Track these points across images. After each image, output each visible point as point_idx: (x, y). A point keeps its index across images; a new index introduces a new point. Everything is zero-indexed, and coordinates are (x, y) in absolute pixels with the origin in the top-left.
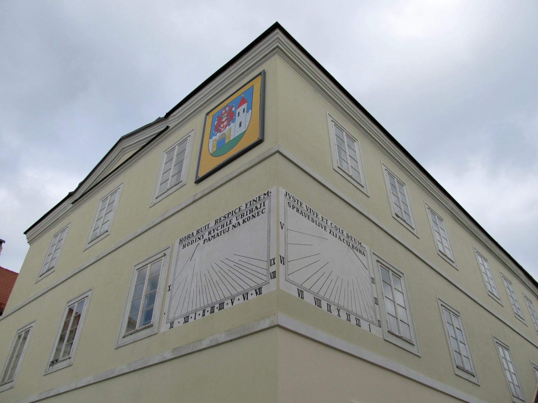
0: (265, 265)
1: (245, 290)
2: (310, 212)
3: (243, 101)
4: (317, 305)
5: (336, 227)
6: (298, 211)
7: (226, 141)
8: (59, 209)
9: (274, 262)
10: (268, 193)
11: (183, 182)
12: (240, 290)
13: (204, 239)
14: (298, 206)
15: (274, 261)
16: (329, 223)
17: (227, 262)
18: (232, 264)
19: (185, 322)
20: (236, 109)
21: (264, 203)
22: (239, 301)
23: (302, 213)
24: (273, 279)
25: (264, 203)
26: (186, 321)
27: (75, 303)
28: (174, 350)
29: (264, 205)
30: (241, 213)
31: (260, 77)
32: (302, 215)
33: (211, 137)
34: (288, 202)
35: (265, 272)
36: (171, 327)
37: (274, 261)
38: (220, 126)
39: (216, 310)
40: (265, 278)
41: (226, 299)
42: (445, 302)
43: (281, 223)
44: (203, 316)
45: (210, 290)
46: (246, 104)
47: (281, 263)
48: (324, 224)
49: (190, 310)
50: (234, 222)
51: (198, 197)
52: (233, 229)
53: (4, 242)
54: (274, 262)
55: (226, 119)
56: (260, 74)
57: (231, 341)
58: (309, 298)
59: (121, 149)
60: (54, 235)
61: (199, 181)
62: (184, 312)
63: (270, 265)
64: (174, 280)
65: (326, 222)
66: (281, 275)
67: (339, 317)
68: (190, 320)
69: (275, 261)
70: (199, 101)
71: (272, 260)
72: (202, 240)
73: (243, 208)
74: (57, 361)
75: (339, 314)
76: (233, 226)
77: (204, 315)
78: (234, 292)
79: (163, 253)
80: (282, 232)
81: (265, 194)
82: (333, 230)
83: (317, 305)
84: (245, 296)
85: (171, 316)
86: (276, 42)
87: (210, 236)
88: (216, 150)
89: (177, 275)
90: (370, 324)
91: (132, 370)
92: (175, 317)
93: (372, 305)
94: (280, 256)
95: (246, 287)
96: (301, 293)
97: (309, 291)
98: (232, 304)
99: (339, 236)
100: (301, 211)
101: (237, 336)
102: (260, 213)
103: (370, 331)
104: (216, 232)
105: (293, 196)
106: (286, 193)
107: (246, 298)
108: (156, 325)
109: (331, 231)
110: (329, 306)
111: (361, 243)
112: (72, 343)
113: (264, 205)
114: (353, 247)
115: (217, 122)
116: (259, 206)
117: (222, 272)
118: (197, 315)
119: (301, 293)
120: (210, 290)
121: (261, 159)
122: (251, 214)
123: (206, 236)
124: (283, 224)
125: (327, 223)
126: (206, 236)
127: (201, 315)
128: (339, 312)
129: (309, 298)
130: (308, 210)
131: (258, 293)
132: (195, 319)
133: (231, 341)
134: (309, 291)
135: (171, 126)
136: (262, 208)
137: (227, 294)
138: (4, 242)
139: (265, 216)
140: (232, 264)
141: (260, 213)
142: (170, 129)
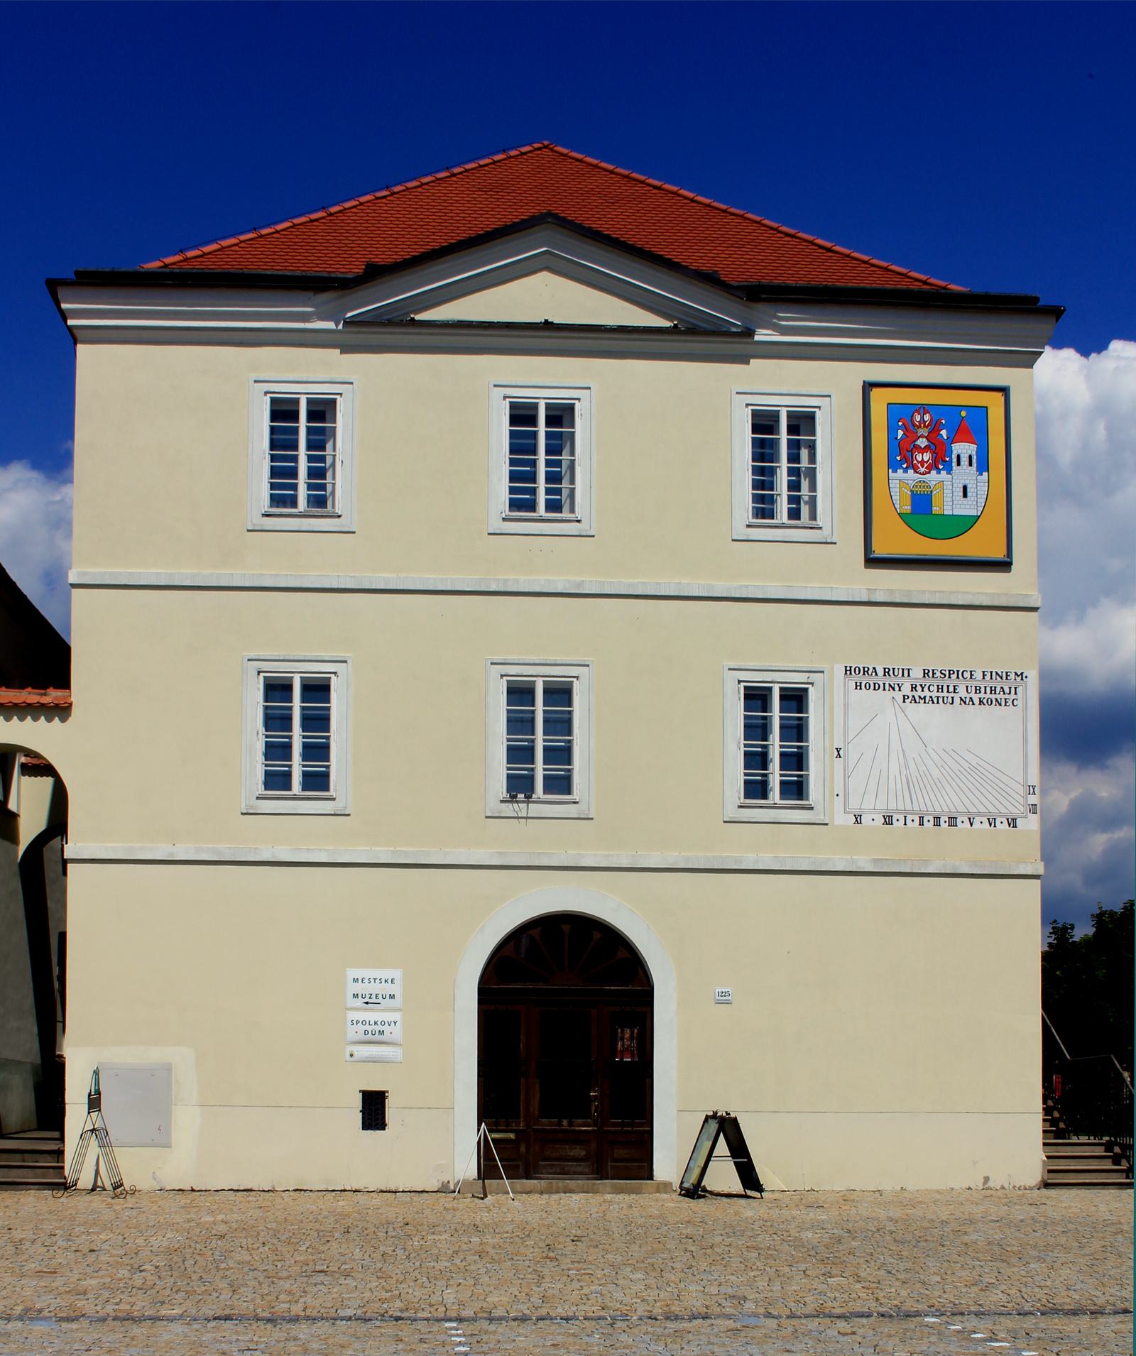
18: (966, 765)
22: (981, 825)
28: (876, 861)
29: (1016, 694)
30: (974, 684)
39: (944, 825)
44: (920, 825)
45: (917, 787)
50: (962, 692)
64: (846, 743)
77: (921, 824)
78: (909, 807)
107: (993, 825)
108: (819, 807)
113: (1016, 694)
119: (858, 820)
123: (906, 689)
131: (1012, 825)
136: (1012, 696)
140: (966, 765)
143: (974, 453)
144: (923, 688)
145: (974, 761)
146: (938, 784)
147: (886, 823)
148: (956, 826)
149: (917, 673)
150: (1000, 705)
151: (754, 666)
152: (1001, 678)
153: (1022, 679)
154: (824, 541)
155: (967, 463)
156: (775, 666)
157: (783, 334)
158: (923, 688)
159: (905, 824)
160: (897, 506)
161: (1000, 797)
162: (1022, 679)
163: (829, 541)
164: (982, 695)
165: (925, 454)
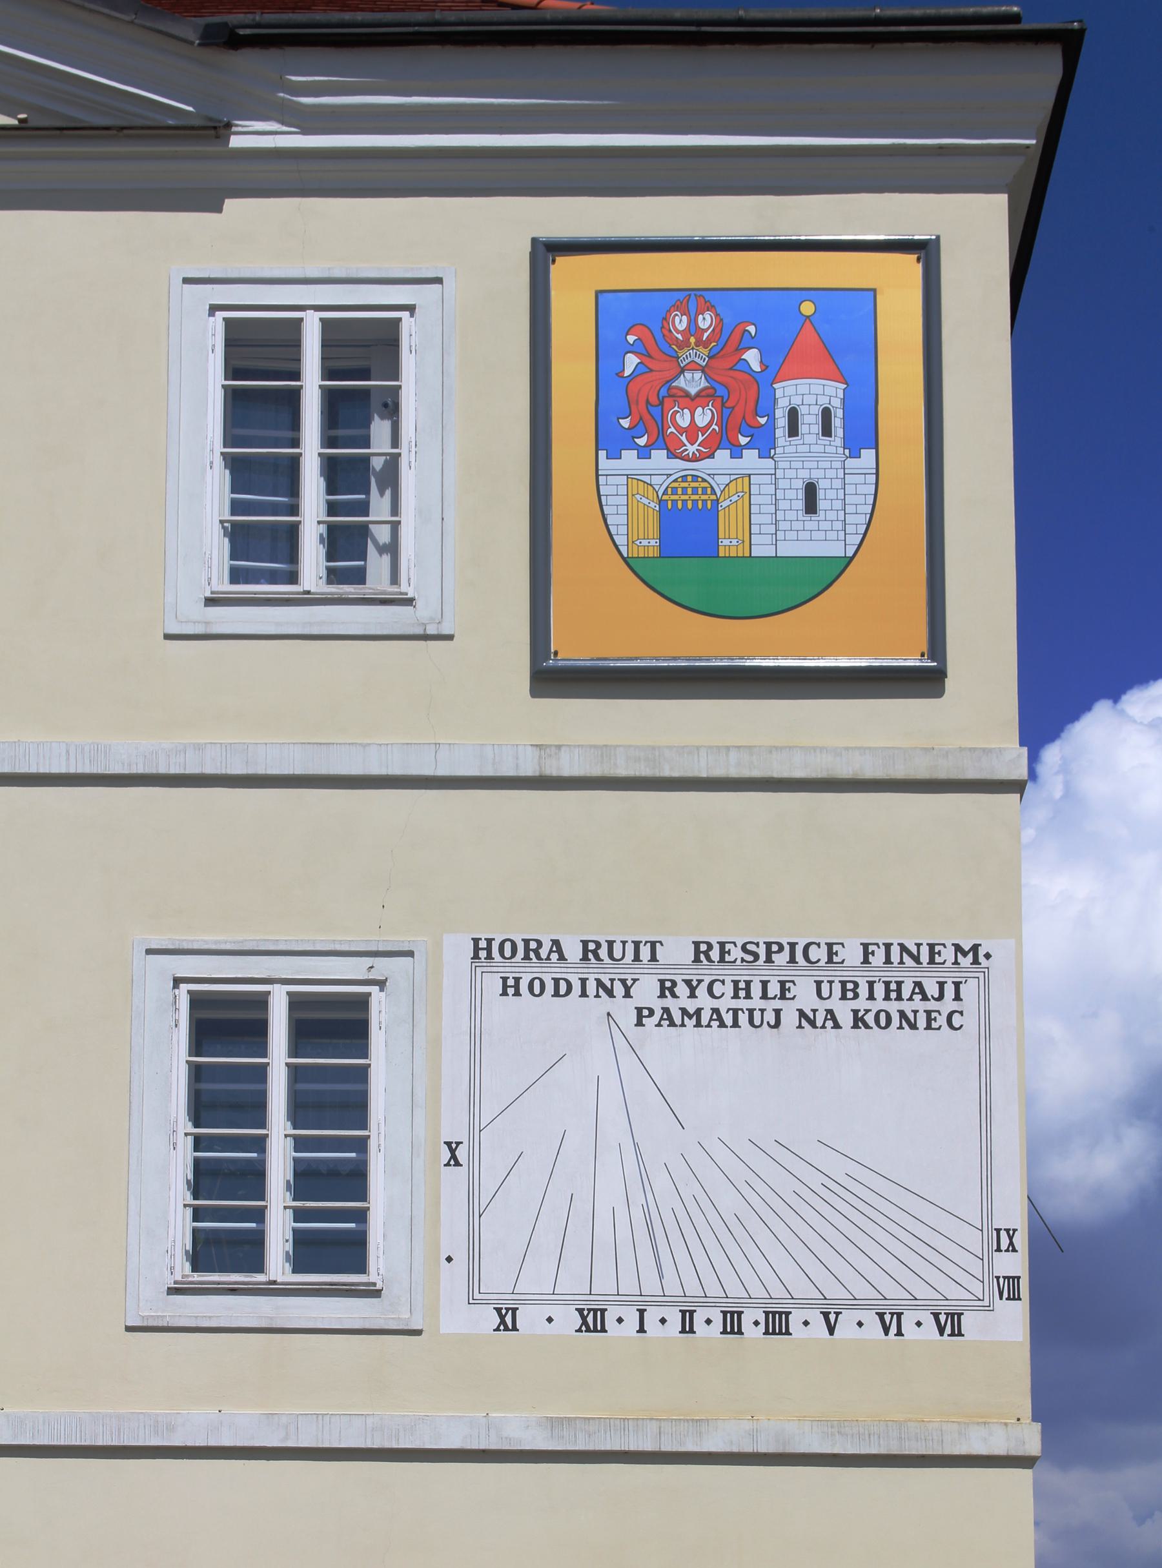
1: (826, 1299)
9: (1011, 1243)
10: (975, 948)
15: (1011, 1238)
18: (815, 1180)
20: (775, 372)
21: (957, 985)
24: (1007, 1299)
25: (957, 985)
28: (554, 1423)
35: (976, 1267)
37: (1011, 1238)
40: (977, 1288)
41: (620, 1298)
45: (675, 1235)
50: (804, 995)
52: (800, 1026)
54: (1011, 1243)
63: (995, 1247)
69: (1014, 1240)
71: (1003, 1234)
73: (851, 954)
76: (802, 1014)
78: (651, 1286)
81: (958, 948)
84: (732, 1323)
98: (831, 1330)
102: (942, 1020)
104: (703, 1000)
111: (19, 740)
116: (932, 989)
120: (675, 1235)
121: (942, 775)
132: (642, 1330)
137: (629, 1286)
139: (966, 1040)
140: (815, 1180)
141: (942, 1020)
143: (836, 403)
145: (837, 1168)
147: (584, 1327)
151: (216, 942)
154: (419, 631)
155: (817, 428)
156: (314, 942)
157: (305, 131)
159: (642, 1330)
160: (621, 540)
163: (431, 630)
165: (699, 410)
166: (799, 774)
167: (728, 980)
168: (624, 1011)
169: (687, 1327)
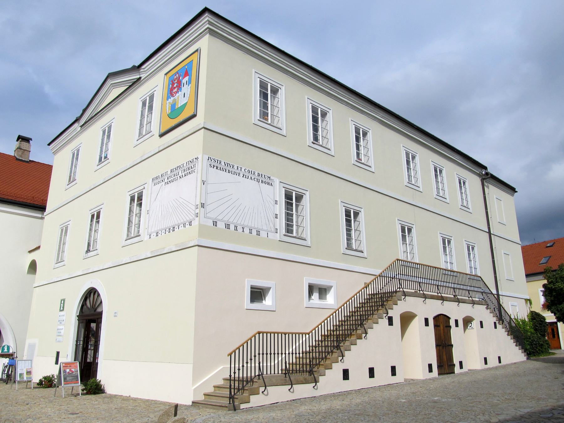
0: (194, 208)
2: (228, 166)
3: (186, 74)
4: (227, 228)
5: (249, 171)
6: (217, 168)
7: (177, 107)
8: (71, 130)
11: (152, 132)
12: (182, 221)
13: (165, 182)
14: (216, 164)
16: (243, 170)
17: (176, 200)
19: (157, 236)
23: (221, 169)
26: (157, 236)
27: (135, 193)
30: (184, 168)
31: (196, 53)
32: (221, 170)
33: (167, 100)
34: (209, 164)
36: (150, 238)
38: (172, 90)
39: (171, 231)
42: (347, 203)
43: (203, 181)
46: (188, 76)
47: (202, 207)
48: (238, 172)
49: (158, 229)
50: (180, 174)
51: (161, 149)
53: (31, 139)
55: (177, 86)
56: (197, 50)
57: (178, 250)
58: (221, 225)
59: (110, 84)
60: (71, 151)
61: (161, 135)
62: (156, 229)
65: (240, 170)
66: (202, 215)
67: (243, 232)
68: (159, 235)
70: (157, 62)
72: (164, 182)
74: (89, 251)
75: (243, 230)
79: (143, 186)
80: (204, 187)
82: (247, 174)
83: (227, 228)
85: (150, 231)
86: (206, 24)
87: (168, 181)
88: (171, 112)
89: (151, 204)
90: (268, 232)
91: (132, 261)
92: (152, 231)
93: (272, 219)
94: (202, 203)
95: (185, 220)
96: (215, 224)
97: (221, 220)
99: (251, 177)
100: (220, 167)
101: (180, 248)
103: (268, 237)
105: (214, 158)
106: (209, 157)
109: (244, 175)
110: (236, 227)
112: (152, 112)
114: (262, 182)
115: (171, 85)
117: (174, 207)
118: (162, 232)
119: (215, 224)
122: (189, 171)
124: (205, 181)
125: (241, 170)
126: (166, 181)
127: (164, 233)
128: (243, 229)
129: (221, 225)
130: (225, 165)
133: (178, 250)
134: (221, 220)
135: (143, 76)
136: (194, 168)
137: (177, 223)
138: (31, 139)
142: (142, 79)
144: (170, 177)
146: (171, 215)
148: (230, 229)
149: (169, 172)
150: (190, 174)
152: (191, 162)
153: (197, 160)
155: (186, 84)
158: (170, 177)
160: (167, 112)
161: (188, 214)
162: (197, 160)
164: (186, 172)
166: (181, 138)
167: (212, 165)
168: (163, 183)
169: (251, 233)
